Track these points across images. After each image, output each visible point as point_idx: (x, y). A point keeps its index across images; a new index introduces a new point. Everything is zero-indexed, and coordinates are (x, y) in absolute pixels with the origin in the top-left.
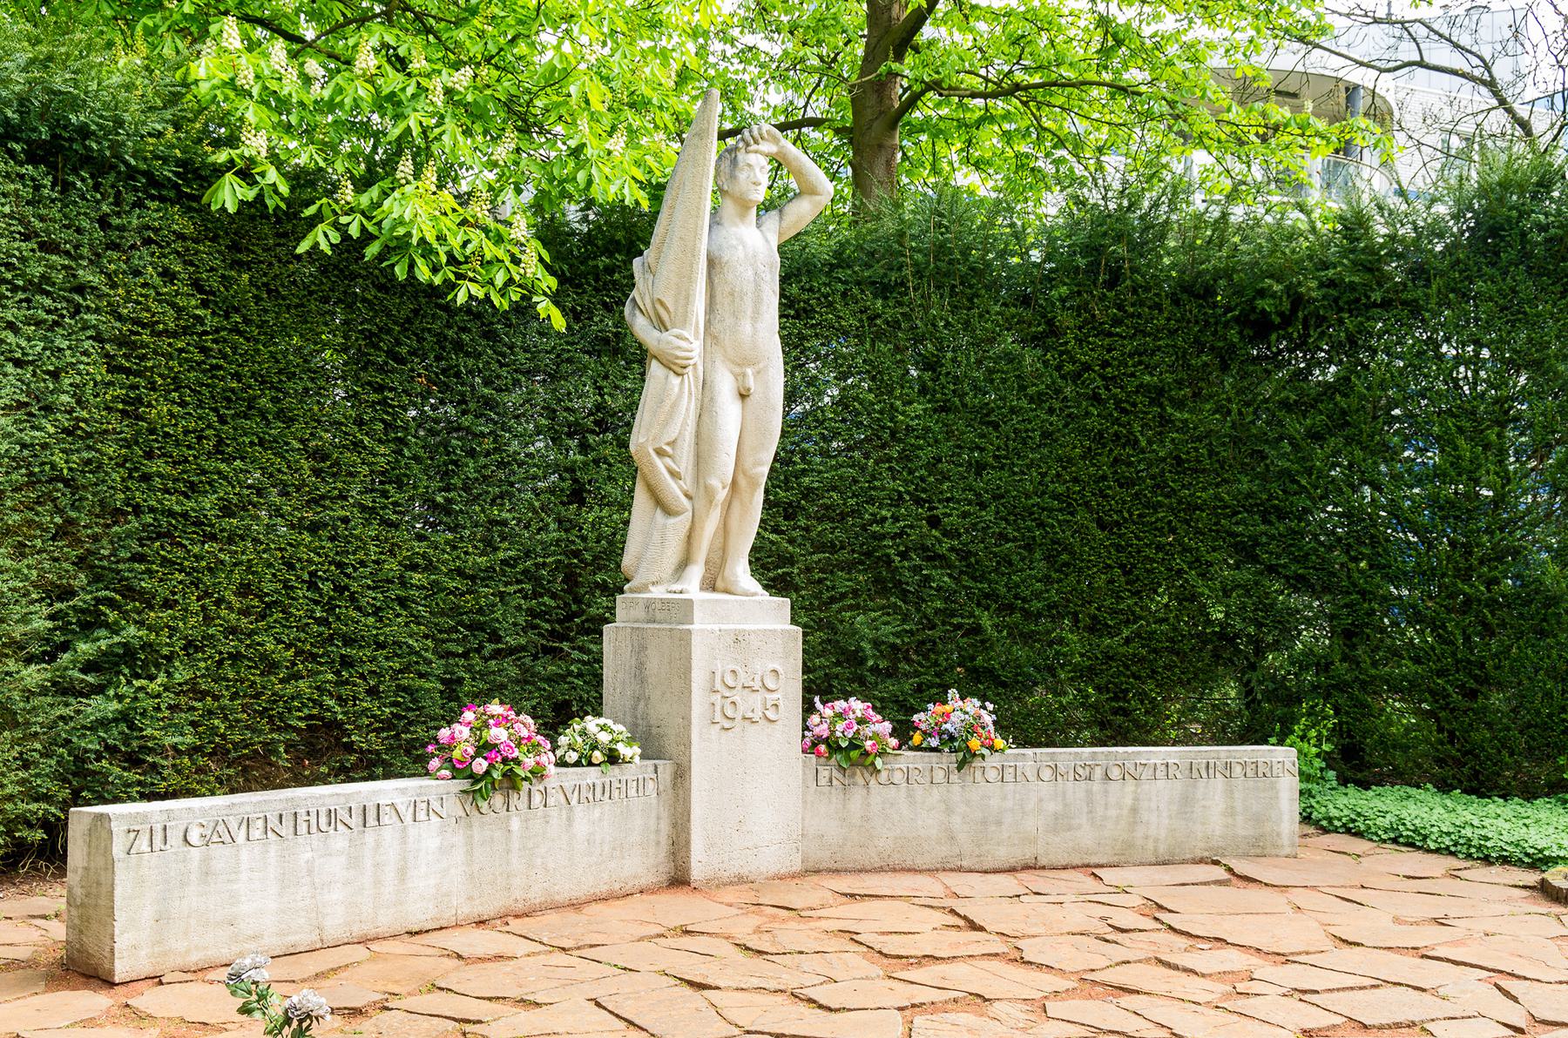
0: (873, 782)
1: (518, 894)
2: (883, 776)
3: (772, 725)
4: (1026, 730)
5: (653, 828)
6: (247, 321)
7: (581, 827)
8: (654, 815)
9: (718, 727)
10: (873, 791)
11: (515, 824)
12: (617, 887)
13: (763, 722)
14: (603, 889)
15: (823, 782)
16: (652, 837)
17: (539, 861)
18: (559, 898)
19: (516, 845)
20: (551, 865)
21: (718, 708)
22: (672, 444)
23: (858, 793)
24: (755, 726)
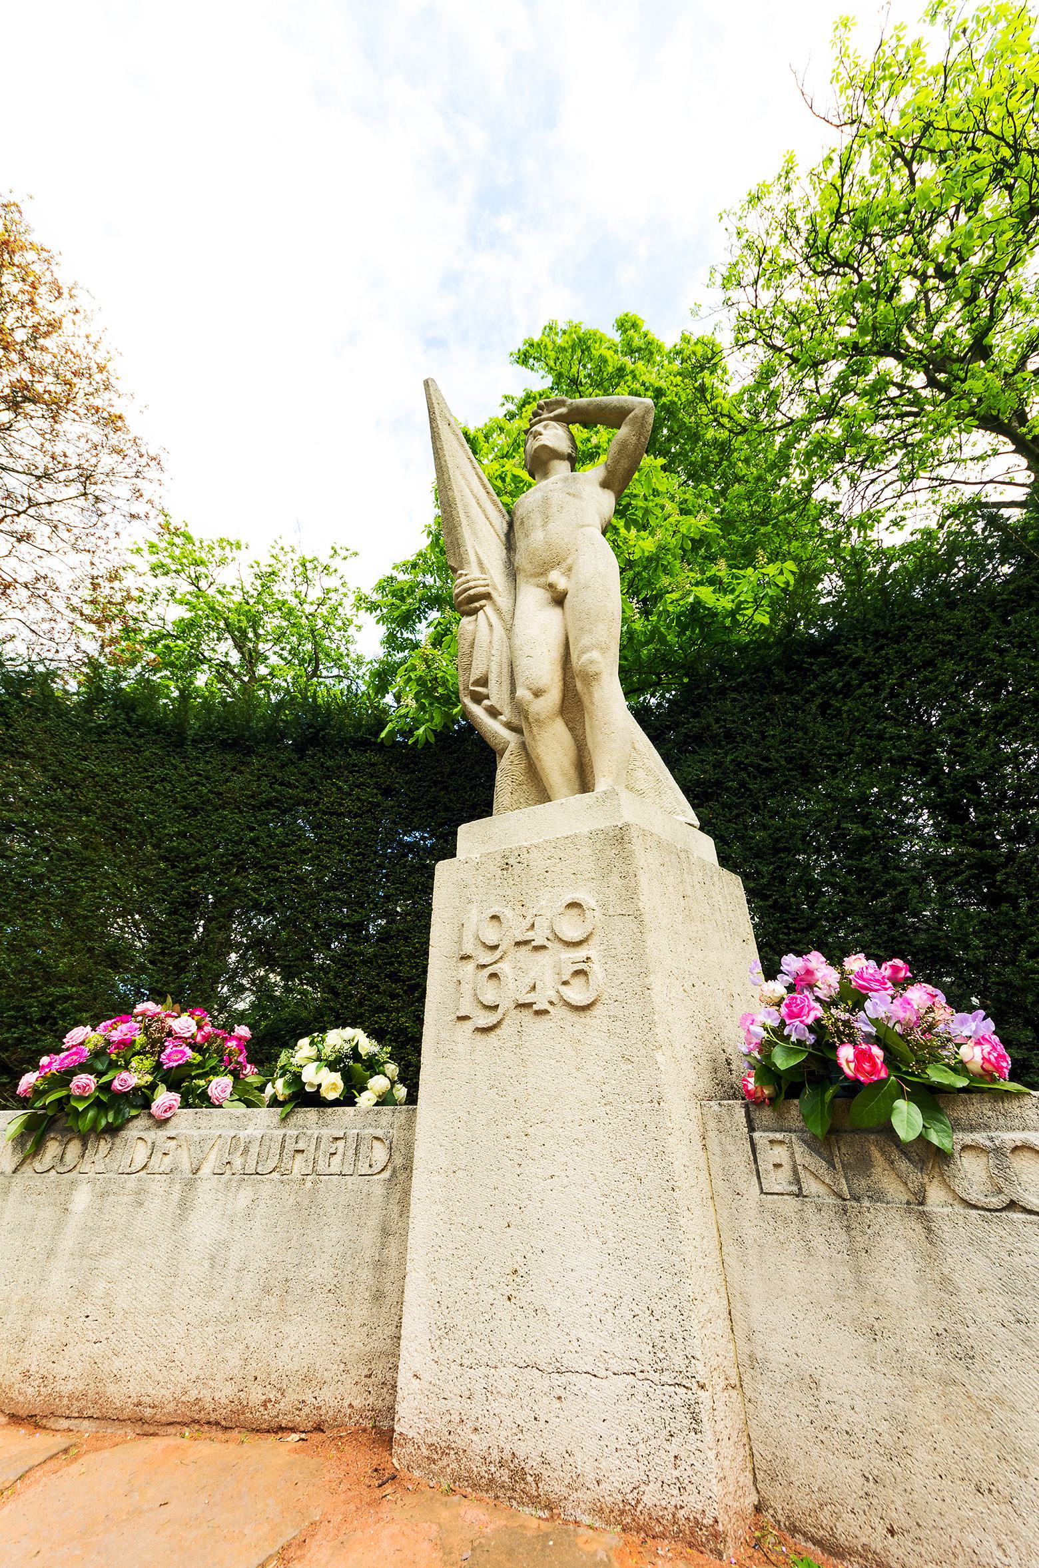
0: (936, 1195)
1: (34, 1360)
2: (972, 1172)
3: (597, 1010)
4: (755, 926)
5: (370, 1253)
6: (827, 739)
7: (204, 1225)
8: (373, 1220)
9: (468, 1026)
10: (945, 1230)
11: (82, 1198)
12: (256, 1395)
13: (558, 1012)
14: (221, 1395)
15: (779, 1181)
16: (365, 1275)
17: (100, 1287)
18: (118, 1394)
19: (68, 1242)
20: (122, 1302)
21: (466, 988)
22: (483, 681)
23: (893, 1232)
24: (543, 1021)
